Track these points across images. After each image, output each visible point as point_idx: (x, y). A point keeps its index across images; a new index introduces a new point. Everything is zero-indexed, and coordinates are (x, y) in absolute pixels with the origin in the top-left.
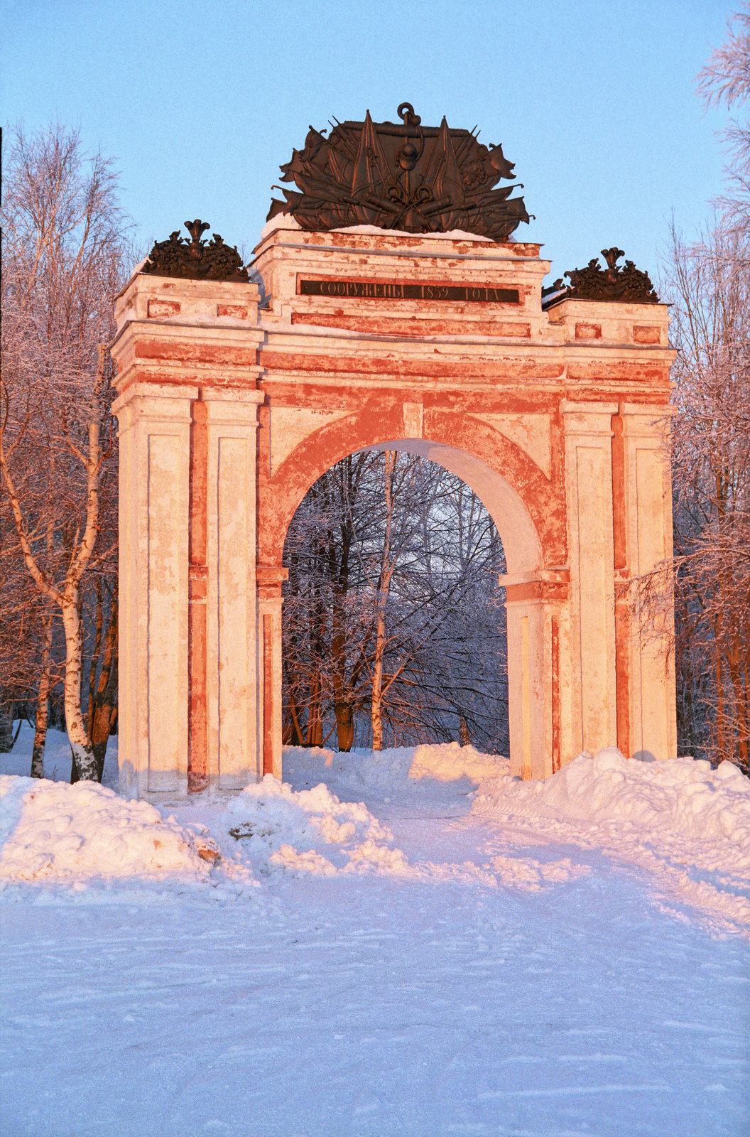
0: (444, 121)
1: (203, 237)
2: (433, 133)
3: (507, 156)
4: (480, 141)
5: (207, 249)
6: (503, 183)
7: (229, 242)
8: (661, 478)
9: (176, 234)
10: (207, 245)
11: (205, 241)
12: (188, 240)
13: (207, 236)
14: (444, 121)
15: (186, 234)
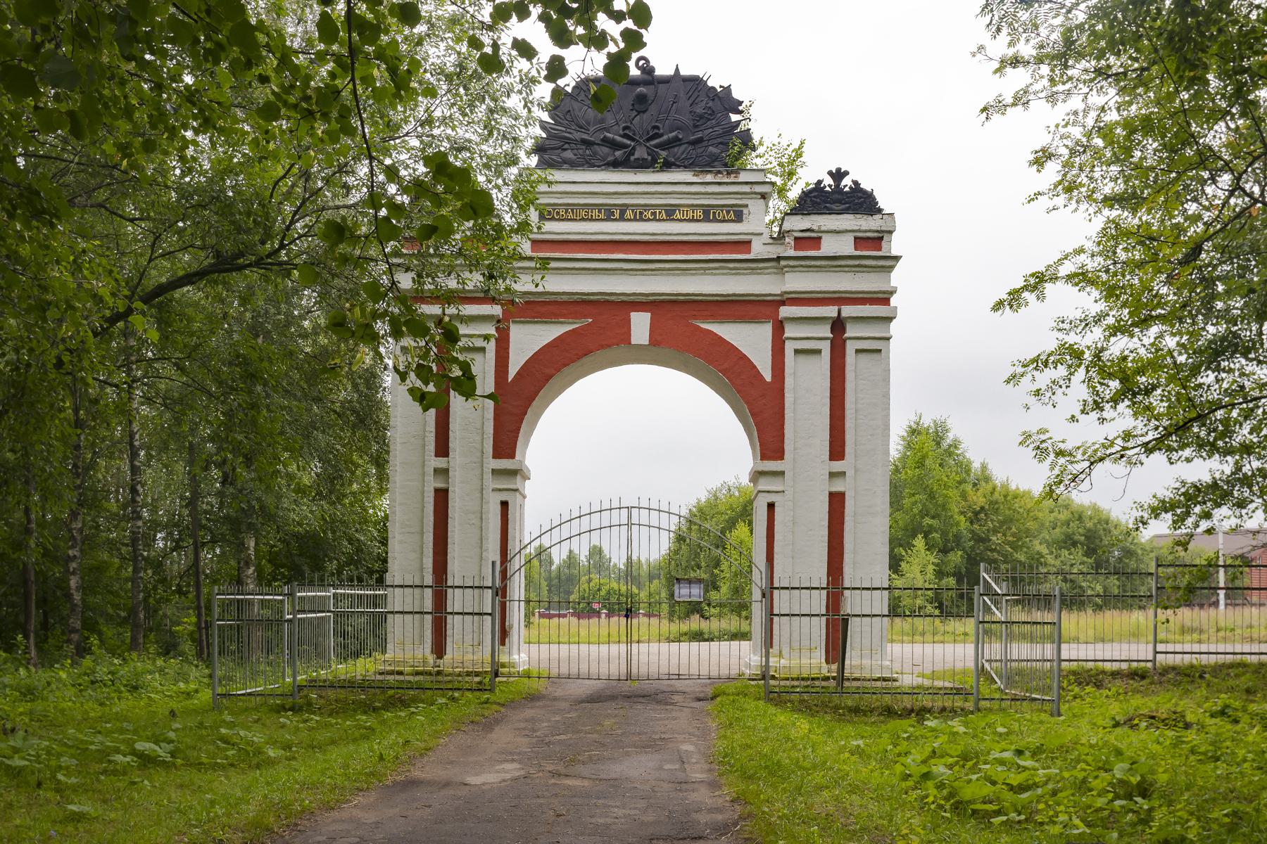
0: (677, 69)
1: (843, 183)
2: (666, 81)
3: (736, 94)
4: (710, 84)
5: (847, 192)
6: (734, 118)
7: (865, 186)
8: (715, 484)
9: (820, 182)
10: (847, 189)
11: (845, 186)
12: (830, 186)
13: (847, 182)
14: (677, 69)
15: (828, 181)
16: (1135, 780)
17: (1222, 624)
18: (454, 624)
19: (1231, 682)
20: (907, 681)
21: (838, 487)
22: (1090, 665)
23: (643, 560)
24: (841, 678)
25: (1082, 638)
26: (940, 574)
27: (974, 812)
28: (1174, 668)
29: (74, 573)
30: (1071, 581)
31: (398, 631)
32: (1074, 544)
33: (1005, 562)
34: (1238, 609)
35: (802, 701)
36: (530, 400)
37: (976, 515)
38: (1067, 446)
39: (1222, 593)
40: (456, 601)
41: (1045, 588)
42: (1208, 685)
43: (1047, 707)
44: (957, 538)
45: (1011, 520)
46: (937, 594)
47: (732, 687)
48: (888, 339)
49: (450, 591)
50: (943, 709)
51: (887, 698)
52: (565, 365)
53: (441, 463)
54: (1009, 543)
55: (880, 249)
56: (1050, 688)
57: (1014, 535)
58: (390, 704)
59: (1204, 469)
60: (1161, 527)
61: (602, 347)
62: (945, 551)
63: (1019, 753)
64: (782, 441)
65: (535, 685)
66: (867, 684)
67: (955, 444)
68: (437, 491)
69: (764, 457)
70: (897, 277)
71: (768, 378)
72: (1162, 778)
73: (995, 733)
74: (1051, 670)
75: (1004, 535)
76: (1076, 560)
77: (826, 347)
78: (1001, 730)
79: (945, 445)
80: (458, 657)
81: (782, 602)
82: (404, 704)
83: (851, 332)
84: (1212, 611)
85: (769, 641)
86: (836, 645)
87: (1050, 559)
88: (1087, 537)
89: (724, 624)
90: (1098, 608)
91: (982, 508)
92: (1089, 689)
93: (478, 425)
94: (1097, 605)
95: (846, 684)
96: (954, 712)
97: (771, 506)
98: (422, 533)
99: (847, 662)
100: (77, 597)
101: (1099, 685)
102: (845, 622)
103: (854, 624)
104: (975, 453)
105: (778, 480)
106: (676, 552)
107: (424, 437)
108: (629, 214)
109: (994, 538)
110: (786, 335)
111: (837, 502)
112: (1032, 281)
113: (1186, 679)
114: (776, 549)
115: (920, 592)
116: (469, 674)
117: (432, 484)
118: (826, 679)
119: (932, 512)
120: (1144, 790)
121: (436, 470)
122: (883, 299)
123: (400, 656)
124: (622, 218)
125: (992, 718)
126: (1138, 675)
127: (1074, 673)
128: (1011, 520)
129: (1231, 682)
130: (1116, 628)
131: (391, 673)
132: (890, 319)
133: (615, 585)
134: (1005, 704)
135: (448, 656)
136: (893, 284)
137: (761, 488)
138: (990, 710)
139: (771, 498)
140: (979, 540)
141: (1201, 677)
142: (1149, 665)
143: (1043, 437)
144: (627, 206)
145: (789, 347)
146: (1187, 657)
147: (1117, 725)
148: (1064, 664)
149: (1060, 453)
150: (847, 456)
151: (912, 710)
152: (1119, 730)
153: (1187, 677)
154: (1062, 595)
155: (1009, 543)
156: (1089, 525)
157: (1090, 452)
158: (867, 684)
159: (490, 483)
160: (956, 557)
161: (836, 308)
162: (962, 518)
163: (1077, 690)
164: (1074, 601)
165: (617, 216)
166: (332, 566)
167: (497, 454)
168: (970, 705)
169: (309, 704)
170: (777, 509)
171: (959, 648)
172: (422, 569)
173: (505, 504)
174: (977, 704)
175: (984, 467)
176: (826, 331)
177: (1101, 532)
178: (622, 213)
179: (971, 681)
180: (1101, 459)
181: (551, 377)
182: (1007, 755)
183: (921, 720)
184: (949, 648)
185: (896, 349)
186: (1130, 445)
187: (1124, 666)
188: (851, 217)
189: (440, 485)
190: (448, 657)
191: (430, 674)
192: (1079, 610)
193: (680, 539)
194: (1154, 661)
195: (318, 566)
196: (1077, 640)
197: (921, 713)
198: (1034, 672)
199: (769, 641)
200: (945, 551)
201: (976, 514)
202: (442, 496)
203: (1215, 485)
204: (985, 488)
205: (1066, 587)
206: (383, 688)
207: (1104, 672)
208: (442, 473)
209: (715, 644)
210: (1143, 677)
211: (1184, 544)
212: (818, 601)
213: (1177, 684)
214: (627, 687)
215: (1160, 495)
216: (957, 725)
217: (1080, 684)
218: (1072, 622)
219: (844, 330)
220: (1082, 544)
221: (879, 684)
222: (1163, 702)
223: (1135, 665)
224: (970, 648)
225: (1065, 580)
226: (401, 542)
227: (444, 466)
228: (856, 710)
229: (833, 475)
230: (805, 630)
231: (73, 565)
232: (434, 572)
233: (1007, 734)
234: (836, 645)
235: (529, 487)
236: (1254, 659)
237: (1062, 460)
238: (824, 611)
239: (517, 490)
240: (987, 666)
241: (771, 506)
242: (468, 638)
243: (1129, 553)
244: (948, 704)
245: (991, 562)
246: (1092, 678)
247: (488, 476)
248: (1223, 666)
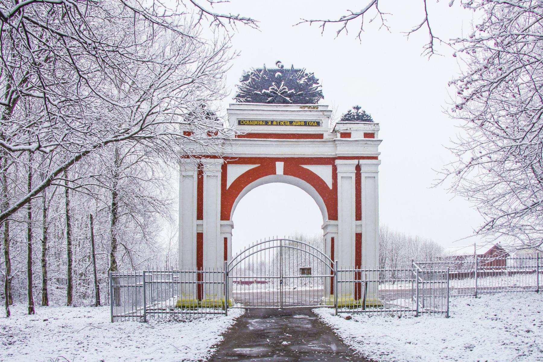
48: (378, 173)
70: (381, 148)
136: (379, 151)
139: (333, 235)
165: (270, 123)
173: (226, 239)
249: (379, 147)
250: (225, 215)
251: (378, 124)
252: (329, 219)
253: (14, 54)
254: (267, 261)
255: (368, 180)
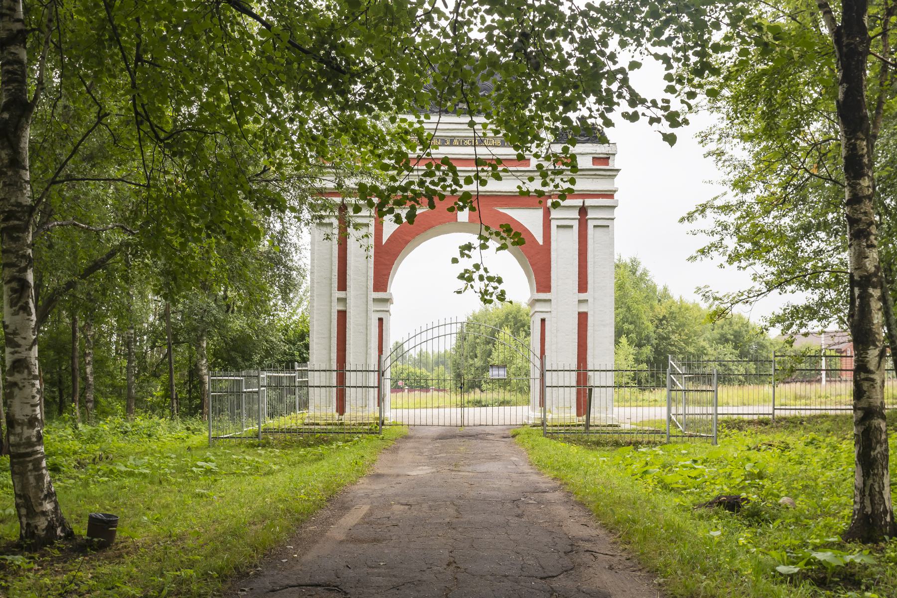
16: (756, 471)
17: (823, 394)
18: (350, 393)
19: (818, 427)
20: (626, 427)
21: (583, 309)
22: (735, 417)
23: (430, 352)
24: (587, 425)
25: (730, 402)
26: (637, 361)
27: (673, 489)
28: (785, 419)
29: (89, 364)
30: (724, 365)
31: (317, 398)
32: (727, 341)
33: (680, 353)
34: (833, 384)
35: (565, 438)
36: (396, 256)
37: (661, 321)
38: (719, 295)
39: (824, 373)
40: (351, 379)
41: (708, 370)
42: (805, 428)
43: (710, 440)
44: (648, 338)
45: (684, 325)
46: (635, 374)
47: (522, 430)
48: (613, 219)
49: (347, 373)
50: (649, 442)
51: (616, 436)
52: (417, 234)
53: (341, 294)
54: (684, 341)
55: (608, 164)
56: (711, 430)
57: (686, 335)
58: (320, 442)
59: (801, 297)
60: (775, 333)
61: (440, 223)
62: (640, 346)
63: (695, 461)
64: (550, 281)
65: (405, 430)
66: (604, 428)
67: (645, 273)
68: (339, 312)
69: (538, 291)
70: (618, 182)
71: (541, 243)
72: (770, 470)
73: (681, 454)
74: (711, 420)
75: (680, 335)
76: (728, 352)
77: (576, 224)
78: (683, 452)
79: (638, 273)
80: (353, 414)
81: (550, 379)
82: (328, 442)
83: (591, 214)
84: (818, 385)
85: (542, 403)
86: (584, 404)
87: (710, 351)
88: (735, 337)
89: (495, 395)
90: (741, 383)
91: (664, 317)
92: (735, 431)
93: (364, 271)
94: (740, 381)
95: (591, 428)
96: (655, 444)
97: (543, 321)
98: (330, 338)
99: (592, 416)
100: (91, 379)
101: (740, 429)
102: (590, 390)
103: (596, 391)
104: (659, 279)
105: (547, 304)
106: (459, 347)
107: (331, 279)
108: (456, 142)
109: (673, 337)
110: (552, 216)
111: (583, 318)
112: (700, 208)
113: (792, 425)
114: (546, 347)
115: (625, 373)
116: (360, 424)
117: (337, 307)
118: (579, 425)
119: (630, 319)
120: (761, 476)
121: (338, 299)
122: (609, 195)
123: (318, 414)
124: (451, 145)
125: (678, 446)
126: (763, 423)
127: (726, 422)
128: (684, 325)
129: (818, 427)
130: (756, 397)
131: (313, 424)
132: (614, 207)
133: (412, 370)
134: (686, 439)
135: (347, 413)
136: (616, 186)
137: (537, 309)
138: (676, 443)
139: (543, 316)
140: (662, 338)
141: (801, 423)
142: (771, 417)
143: (707, 290)
144: (455, 137)
145: (554, 224)
146: (793, 412)
147: (749, 449)
148: (719, 417)
149: (715, 299)
150: (589, 290)
151: (631, 443)
152: (751, 452)
153: (793, 423)
154: (718, 374)
155: (684, 341)
156: (736, 328)
157: (731, 298)
158: (604, 428)
159: (372, 307)
160: (647, 350)
161: (581, 201)
162: (649, 324)
163: (727, 431)
164: (725, 378)
165: (448, 143)
166: (256, 358)
167: (376, 289)
168: (664, 440)
169: (268, 443)
170: (546, 322)
171: (658, 409)
172: (330, 360)
173: (381, 320)
174: (668, 439)
175: (665, 289)
176: (575, 214)
177: (744, 333)
178: (452, 141)
179: (663, 428)
180: (737, 302)
181: (409, 241)
182: (689, 463)
183: (636, 448)
184: (646, 409)
185: (618, 226)
186: (751, 295)
187: (756, 417)
188: (590, 145)
189: (341, 308)
190: (347, 414)
191: (336, 425)
192: (729, 384)
193: (463, 338)
194: (773, 414)
195: (247, 357)
196: (728, 404)
197: (636, 444)
198: (701, 421)
199: (542, 403)
200: (640, 346)
201: (661, 320)
202: (342, 316)
203: (807, 307)
204: (666, 303)
205: (721, 369)
206: (313, 433)
207: (743, 421)
208: (343, 300)
209: (489, 409)
210: (766, 424)
211: (791, 343)
212: (573, 378)
213: (786, 428)
214: (458, 431)
215: (776, 313)
216: (658, 450)
217: (729, 428)
218: (725, 392)
219: (586, 214)
220: (732, 341)
221: (610, 428)
222: (778, 437)
223: (761, 416)
224: (665, 409)
225: (720, 365)
226: (317, 344)
227: (343, 296)
228: (598, 443)
229: (580, 301)
230: (561, 397)
231: (89, 359)
232: (338, 362)
233: (687, 454)
234: (584, 404)
235: (392, 308)
236: (833, 413)
237: (717, 302)
238: (574, 384)
239: (388, 311)
240: (673, 418)
241: (543, 321)
242: (359, 403)
243: (761, 346)
244: (652, 439)
245: (673, 353)
246: (737, 425)
247: (371, 302)
248: (815, 417)
249: (616, 179)
250: (381, 282)
251: (614, 144)
252: (549, 291)
253: (79, 198)
254: (430, 352)
255: (561, 231)
